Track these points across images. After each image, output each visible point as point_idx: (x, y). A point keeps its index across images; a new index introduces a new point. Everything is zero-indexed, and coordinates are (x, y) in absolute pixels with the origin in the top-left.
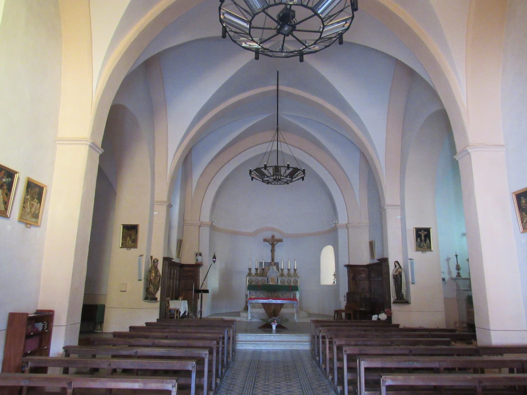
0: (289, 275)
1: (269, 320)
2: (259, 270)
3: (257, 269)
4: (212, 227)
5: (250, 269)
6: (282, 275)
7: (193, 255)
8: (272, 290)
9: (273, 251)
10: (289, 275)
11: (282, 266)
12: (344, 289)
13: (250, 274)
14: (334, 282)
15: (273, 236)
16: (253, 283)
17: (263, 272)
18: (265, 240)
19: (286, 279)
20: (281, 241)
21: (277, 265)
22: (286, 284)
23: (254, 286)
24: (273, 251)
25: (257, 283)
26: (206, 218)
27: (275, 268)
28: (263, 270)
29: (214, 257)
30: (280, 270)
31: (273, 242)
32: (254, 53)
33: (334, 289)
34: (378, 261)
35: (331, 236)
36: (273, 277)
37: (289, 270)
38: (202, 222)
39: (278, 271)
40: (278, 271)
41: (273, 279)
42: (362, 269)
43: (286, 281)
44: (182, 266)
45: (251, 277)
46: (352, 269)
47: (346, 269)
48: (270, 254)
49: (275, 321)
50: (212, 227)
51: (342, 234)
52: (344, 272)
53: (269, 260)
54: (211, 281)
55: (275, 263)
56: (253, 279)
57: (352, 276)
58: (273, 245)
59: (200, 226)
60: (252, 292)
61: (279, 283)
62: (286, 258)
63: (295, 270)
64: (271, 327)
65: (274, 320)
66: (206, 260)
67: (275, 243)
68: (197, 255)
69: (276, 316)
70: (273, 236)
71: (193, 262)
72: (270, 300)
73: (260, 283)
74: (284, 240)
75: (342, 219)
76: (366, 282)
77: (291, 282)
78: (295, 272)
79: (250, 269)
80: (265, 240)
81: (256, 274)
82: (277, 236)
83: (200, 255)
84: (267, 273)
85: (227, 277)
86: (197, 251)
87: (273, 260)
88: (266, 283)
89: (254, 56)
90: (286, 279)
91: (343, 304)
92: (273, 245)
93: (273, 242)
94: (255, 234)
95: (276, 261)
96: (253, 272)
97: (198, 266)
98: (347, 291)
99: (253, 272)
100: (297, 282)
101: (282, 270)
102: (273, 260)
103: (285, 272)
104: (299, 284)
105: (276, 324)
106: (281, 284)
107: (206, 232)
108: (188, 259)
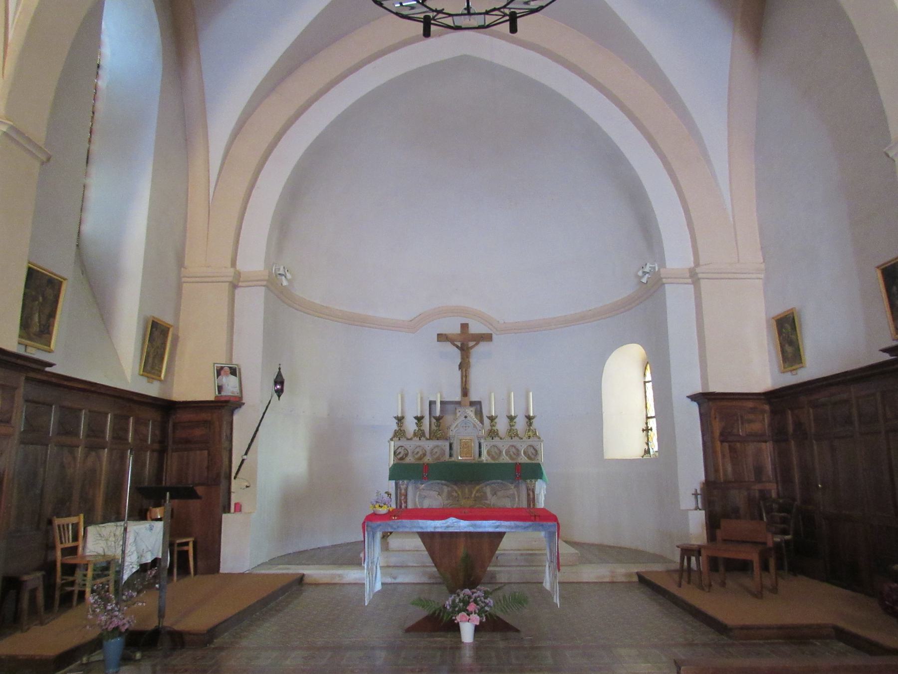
0: (512, 433)
1: (448, 603)
2: (426, 422)
3: (419, 419)
4: (277, 290)
5: (400, 420)
6: (493, 434)
7: (211, 373)
8: (464, 477)
9: (464, 366)
10: (512, 433)
11: (491, 408)
12: (692, 472)
13: (399, 434)
14: (647, 452)
15: (464, 326)
16: (410, 460)
17: (437, 422)
18: (442, 337)
19: (504, 445)
20: (488, 338)
21: (477, 405)
22: (505, 459)
23: (427, 467)
24: (464, 366)
25: (420, 458)
26: (253, 259)
27: (471, 412)
28: (438, 419)
29: (279, 380)
30: (487, 421)
31: (465, 343)
32: (422, 24)
33: (655, 470)
34: (887, 357)
35: (641, 311)
36: (466, 439)
37: (511, 418)
38: (238, 274)
39: (482, 421)
40: (482, 421)
41: (466, 446)
42: (750, 404)
43: (503, 451)
44: (167, 408)
45: (403, 442)
46: (719, 409)
47: (695, 406)
48: (458, 374)
49: (472, 607)
50: (277, 290)
51: (678, 301)
52: (689, 418)
53: (457, 397)
54: (273, 457)
55: (472, 404)
56: (411, 445)
57: (717, 427)
58: (465, 350)
59: (234, 286)
60: (403, 484)
61: (485, 458)
62: (504, 386)
63: (529, 418)
64: (455, 628)
65: (466, 603)
66: (255, 388)
67: (471, 344)
68: (219, 372)
69: (472, 583)
70: (464, 326)
71: (209, 395)
72: (452, 520)
73: (428, 459)
74: (494, 336)
75: (677, 255)
76: (768, 449)
77: (518, 453)
78: (530, 424)
79: (400, 420)
80: (442, 337)
81: (419, 434)
82: (476, 328)
83: (233, 372)
84: (448, 428)
85: (332, 442)
86: (222, 360)
87: (465, 392)
88: (447, 458)
89: (421, 31)
90: (504, 445)
91: (695, 525)
92: (465, 350)
93: (465, 343)
94: (413, 326)
95: (474, 397)
96: (411, 426)
97: (224, 407)
98: (703, 478)
99: (411, 426)
100: (536, 452)
101: (492, 419)
102: (465, 392)
103: (502, 426)
104: (542, 459)
105: (476, 619)
106: (490, 461)
107: (252, 305)
108: (190, 383)
